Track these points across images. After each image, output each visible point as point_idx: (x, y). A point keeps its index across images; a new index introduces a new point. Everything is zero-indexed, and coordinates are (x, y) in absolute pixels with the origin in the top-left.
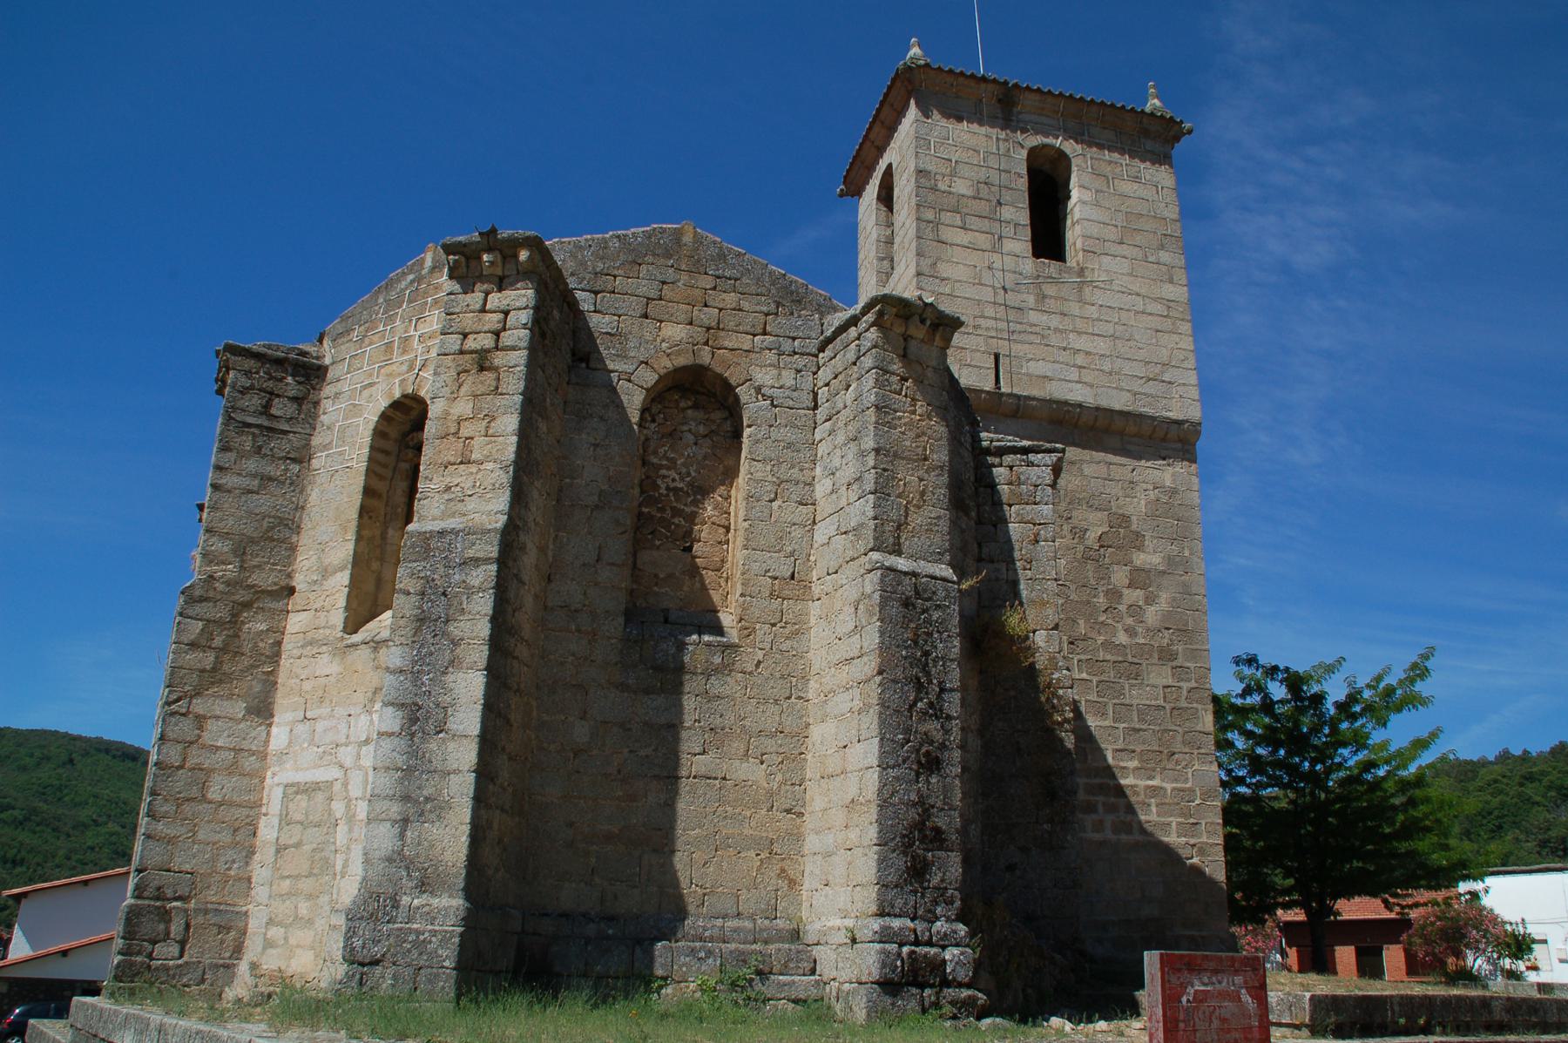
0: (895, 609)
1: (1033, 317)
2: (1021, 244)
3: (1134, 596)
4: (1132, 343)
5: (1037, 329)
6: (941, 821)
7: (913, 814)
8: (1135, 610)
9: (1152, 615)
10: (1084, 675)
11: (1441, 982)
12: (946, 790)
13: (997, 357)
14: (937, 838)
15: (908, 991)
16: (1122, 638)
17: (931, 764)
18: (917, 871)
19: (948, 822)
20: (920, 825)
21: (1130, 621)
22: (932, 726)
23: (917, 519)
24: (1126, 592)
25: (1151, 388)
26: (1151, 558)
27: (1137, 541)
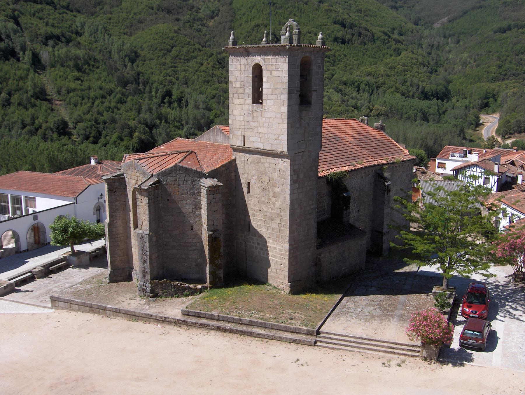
0: (139, 239)
1: (252, 124)
2: (249, 101)
3: (274, 199)
4: (272, 129)
5: (252, 127)
6: (146, 270)
7: (143, 269)
8: (274, 204)
9: (278, 204)
10: (262, 219)
11: (373, 317)
12: (147, 266)
13: (244, 136)
14: (147, 272)
15: (385, 240)
16: (270, 211)
17: (145, 262)
18: (144, 276)
19: (148, 270)
20: (144, 270)
21: (272, 206)
22: (145, 257)
23: (144, 224)
24: (272, 198)
25: (276, 142)
26: (277, 190)
27: (274, 185)
